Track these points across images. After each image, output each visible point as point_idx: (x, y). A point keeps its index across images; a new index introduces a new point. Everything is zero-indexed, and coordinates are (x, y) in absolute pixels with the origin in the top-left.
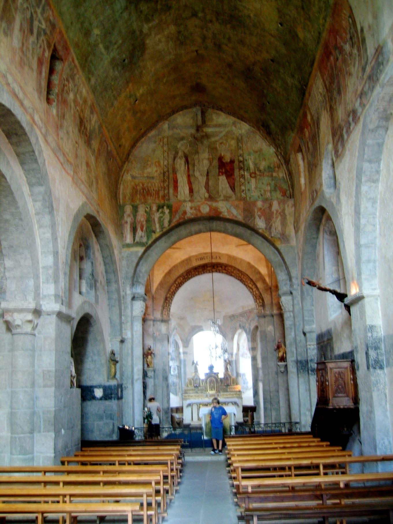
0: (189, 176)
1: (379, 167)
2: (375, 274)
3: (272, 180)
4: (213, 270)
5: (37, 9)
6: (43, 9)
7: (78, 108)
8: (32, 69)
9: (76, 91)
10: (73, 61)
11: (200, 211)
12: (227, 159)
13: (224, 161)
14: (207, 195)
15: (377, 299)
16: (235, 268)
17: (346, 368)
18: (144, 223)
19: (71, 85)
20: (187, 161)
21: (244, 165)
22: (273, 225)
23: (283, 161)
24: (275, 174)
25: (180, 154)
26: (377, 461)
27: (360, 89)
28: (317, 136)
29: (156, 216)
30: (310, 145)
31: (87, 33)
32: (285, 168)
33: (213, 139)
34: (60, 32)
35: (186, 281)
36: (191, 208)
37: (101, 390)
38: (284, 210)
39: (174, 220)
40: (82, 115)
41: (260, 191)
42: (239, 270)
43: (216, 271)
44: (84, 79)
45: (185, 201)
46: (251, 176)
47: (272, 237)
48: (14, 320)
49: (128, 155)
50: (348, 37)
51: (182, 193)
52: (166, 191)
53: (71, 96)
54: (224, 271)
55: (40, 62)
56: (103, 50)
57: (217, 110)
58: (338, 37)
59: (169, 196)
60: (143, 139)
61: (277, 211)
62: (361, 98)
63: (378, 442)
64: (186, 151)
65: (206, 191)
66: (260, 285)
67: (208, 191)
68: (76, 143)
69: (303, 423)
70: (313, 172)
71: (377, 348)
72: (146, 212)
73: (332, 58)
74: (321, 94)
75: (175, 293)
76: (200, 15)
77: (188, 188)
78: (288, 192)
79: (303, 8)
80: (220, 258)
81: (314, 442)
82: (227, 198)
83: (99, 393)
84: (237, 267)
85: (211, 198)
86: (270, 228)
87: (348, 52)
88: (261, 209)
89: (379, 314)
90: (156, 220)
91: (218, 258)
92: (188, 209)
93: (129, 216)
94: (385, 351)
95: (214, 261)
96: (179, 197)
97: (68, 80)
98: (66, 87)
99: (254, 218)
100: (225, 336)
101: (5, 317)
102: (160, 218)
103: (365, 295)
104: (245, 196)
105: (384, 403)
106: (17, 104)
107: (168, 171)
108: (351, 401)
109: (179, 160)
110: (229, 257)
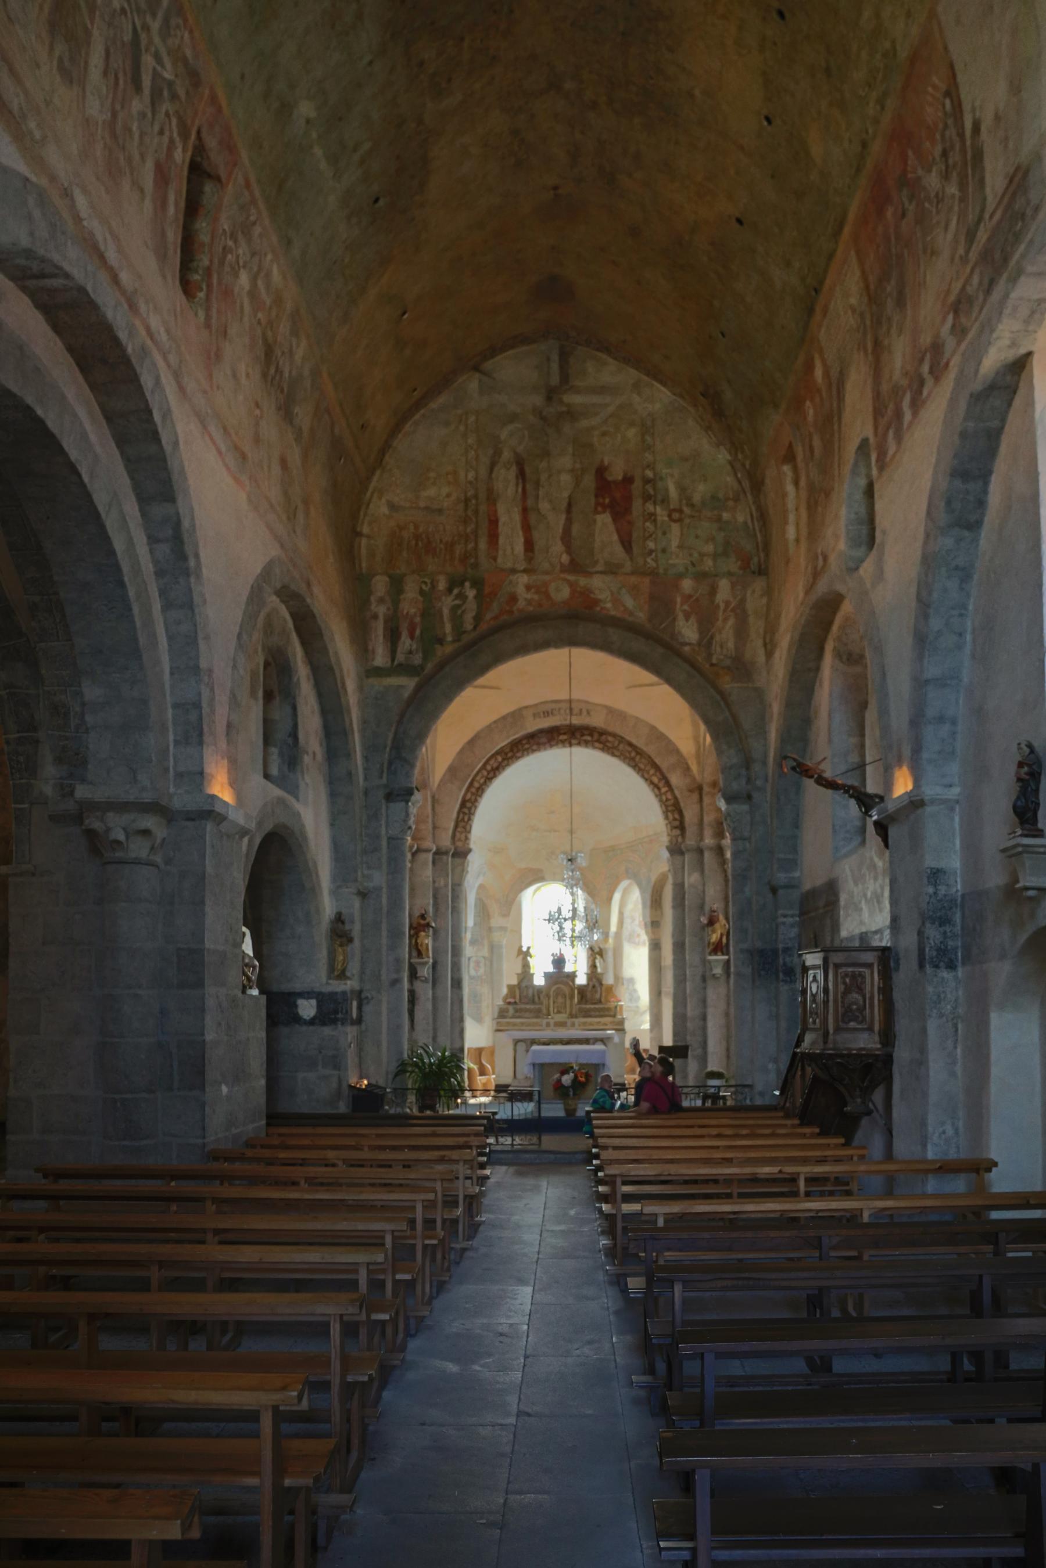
0: (525, 511)
1: (985, 492)
2: (953, 753)
3: (720, 529)
4: (574, 741)
5: (149, 19)
6: (166, 21)
7: (260, 315)
8: (142, 191)
9: (255, 269)
10: (248, 185)
11: (548, 596)
12: (616, 474)
13: (610, 478)
14: (565, 559)
15: (952, 809)
16: (623, 738)
17: (870, 966)
18: (418, 620)
19: (243, 250)
20: (522, 474)
21: (654, 489)
22: (717, 638)
23: (746, 484)
24: (726, 516)
25: (507, 455)
26: (927, 1171)
27: (957, 286)
28: (836, 419)
29: (447, 603)
30: (817, 442)
31: (285, 110)
32: (751, 502)
33: (584, 423)
34: (214, 99)
35: (508, 765)
36: (528, 588)
37: (314, 1002)
38: (743, 601)
39: (488, 616)
40: (269, 334)
41: (691, 555)
42: (630, 744)
43: (579, 744)
44: (274, 239)
45: (514, 571)
46: (670, 516)
47: (712, 665)
48: (108, 830)
49: (383, 452)
50: (938, 150)
51: (509, 551)
52: (471, 546)
53: (244, 279)
54: (597, 745)
55: (162, 176)
56: (323, 165)
57: (598, 350)
58: (910, 153)
59: (477, 558)
60: (417, 417)
61: (727, 603)
62: (956, 312)
63: (930, 1129)
64: (520, 449)
65: (563, 548)
66: (675, 779)
67: (569, 549)
68: (257, 405)
69: (759, 1087)
70: (820, 509)
71: (944, 921)
72: (422, 592)
73: (889, 213)
74: (854, 311)
75: (483, 791)
76: (568, 85)
77: (522, 540)
78: (756, 559)
79: (828, 71)
80: (588, 713)
81: (785, 1126)
82: (612, 570)
83: (307, 1009)
84: (628, 738)
85: (575, 567)
86: (710, 643)
87: (933, 194)
88: (690, 596)
89: (954, 845)
90: (446, 612)
91: (585, 713)
92: (521, 590)
93: (381, 600)
94: (963, 929)
95: (576, 721)
96: (499, 560)
97: (233, 236)
98: (229, 256)
99: (674, 619)
100: (591, 892)
101: (87, 822)
102: (454, 609)
103: (926, 798)
104: (654, 565)
105: (950, 1043)
106: (103, 276)
107: (476, 497)
108: (877, 1038)
109: (503, 471)
110: (610, 711)
